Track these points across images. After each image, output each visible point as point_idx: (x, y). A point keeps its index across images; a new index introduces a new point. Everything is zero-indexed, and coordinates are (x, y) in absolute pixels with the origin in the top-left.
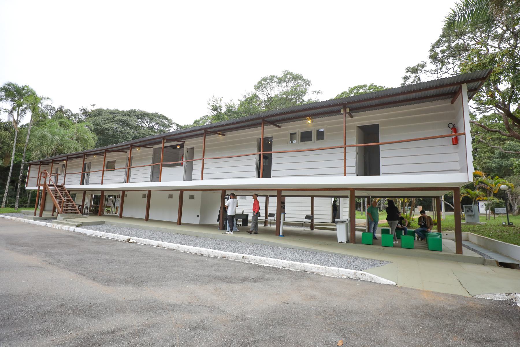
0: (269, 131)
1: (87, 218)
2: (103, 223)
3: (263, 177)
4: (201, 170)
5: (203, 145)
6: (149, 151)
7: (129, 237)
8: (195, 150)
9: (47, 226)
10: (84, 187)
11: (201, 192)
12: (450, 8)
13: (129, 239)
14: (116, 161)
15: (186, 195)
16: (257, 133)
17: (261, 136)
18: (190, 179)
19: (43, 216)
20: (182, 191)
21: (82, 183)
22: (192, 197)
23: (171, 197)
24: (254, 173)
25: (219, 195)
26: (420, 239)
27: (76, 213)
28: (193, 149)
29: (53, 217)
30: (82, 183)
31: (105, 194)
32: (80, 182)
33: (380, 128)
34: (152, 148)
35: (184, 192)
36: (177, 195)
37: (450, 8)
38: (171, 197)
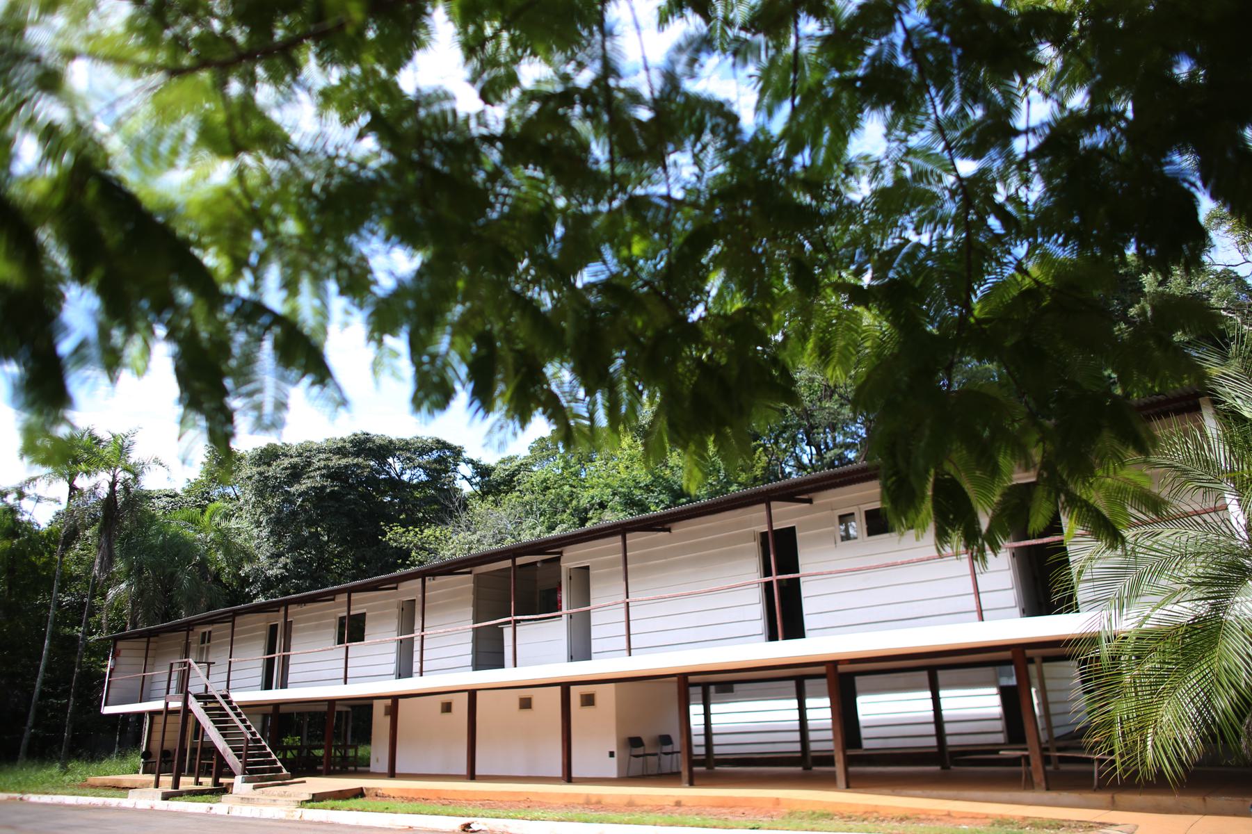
0: (785, 515)
1: (304, 782)
2: (359, 793)
3: (787, 637)
4: (624, 625)
5: (621, 555)
6: (464, 583)
7: (466, 820)
8: (592, 572)
9: (213, 812)
10: (276, 695)
11: (612, 685)
12: (179, 439)
13: (468, 826)
14: (368, 614)
15: (576, 692)
16: (755, 520)
17: (765, 529)
18: (587, 656)
19: (182, 788)
20: (566, 687)
21: (404, 671)
22: (588, 700)
23: (526, 704)
24: (760, 626)
25: (673, 688)
26: (319, 768)
27: (271, 770)
28: (587, 568)
29: (198, 787)
30: (268, 685)
31: (338, 708)
32: (259, 680)
33: (799, 535)
34: (470, 573)
35: (478, 692)
36: (461, 702)
37: (179, 439)
38: (447, 708)
